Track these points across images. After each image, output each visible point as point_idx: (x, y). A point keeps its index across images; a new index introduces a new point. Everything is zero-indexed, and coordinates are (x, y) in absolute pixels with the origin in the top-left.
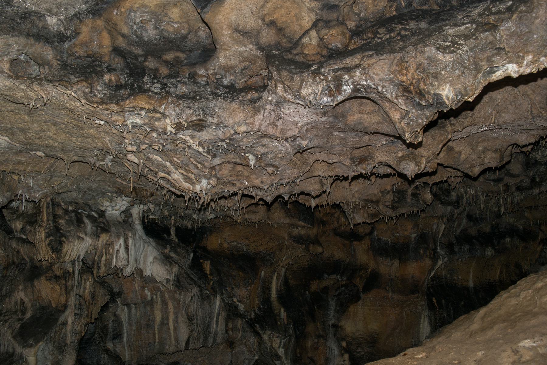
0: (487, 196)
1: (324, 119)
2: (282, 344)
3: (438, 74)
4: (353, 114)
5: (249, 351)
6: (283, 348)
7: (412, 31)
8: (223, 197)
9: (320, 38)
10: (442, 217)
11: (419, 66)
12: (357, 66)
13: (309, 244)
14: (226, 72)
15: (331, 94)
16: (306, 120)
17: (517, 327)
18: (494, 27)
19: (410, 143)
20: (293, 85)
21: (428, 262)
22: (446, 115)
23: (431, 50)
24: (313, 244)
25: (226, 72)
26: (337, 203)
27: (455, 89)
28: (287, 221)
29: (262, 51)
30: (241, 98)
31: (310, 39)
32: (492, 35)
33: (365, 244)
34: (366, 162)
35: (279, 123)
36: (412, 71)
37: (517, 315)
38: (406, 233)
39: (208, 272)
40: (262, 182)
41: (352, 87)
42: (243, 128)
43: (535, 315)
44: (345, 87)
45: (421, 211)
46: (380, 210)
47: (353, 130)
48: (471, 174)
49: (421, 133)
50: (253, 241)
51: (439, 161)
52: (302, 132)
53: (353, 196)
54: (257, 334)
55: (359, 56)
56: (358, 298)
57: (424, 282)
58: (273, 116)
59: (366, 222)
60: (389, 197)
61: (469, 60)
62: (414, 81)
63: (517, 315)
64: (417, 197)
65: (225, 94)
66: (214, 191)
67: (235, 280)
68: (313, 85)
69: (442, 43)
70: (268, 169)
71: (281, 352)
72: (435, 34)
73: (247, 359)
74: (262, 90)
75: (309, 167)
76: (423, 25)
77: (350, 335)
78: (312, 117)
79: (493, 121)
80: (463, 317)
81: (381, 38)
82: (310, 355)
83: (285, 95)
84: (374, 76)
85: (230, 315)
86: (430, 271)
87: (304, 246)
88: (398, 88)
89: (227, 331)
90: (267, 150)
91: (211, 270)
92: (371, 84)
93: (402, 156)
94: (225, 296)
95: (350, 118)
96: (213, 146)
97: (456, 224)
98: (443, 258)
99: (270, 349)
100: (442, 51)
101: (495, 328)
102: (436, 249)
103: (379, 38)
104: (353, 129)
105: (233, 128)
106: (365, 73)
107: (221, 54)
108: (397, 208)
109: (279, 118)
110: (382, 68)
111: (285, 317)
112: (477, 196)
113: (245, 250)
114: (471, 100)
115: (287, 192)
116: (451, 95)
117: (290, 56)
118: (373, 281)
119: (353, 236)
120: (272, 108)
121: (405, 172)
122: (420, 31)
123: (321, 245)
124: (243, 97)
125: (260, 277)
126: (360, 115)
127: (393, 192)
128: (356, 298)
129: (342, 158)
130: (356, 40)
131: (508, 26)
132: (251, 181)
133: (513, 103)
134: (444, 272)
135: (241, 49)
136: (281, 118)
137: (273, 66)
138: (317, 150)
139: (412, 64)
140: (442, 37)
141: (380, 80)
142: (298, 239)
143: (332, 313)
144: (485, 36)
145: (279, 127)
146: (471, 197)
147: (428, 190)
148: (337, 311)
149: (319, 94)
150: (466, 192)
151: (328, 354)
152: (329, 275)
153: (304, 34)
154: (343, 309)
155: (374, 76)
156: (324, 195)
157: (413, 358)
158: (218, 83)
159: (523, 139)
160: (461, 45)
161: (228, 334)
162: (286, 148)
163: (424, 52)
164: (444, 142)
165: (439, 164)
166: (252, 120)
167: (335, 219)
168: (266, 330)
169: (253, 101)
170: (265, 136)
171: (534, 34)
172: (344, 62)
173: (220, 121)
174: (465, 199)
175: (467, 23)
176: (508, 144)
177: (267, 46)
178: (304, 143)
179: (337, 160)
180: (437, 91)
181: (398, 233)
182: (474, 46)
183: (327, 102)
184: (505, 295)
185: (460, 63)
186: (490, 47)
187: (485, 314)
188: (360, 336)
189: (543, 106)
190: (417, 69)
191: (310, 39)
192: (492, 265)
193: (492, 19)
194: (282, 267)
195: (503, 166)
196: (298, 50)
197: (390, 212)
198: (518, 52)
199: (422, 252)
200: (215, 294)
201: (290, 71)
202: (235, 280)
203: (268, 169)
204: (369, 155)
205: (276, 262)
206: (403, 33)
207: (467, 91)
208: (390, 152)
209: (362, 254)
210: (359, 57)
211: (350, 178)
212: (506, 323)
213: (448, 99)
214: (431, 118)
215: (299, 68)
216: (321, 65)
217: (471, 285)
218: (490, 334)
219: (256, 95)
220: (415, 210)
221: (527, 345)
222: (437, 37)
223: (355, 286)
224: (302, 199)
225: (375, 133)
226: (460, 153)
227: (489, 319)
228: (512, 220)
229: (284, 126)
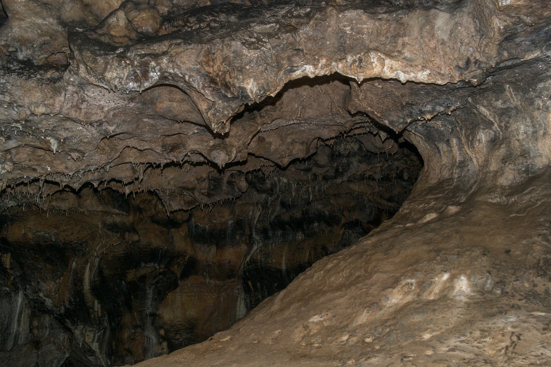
0: (298, 184)
1: (132, 105)
2: (96, 338)
3: (243, 68)
4: (163, 101)
5: (59, 349)
6: (97, 342)
7: (221, 24)
8: (22, 183)
9: (128, 19)
10: (257, 204)
11: (225, 59)
12: (164, 53)
13: (124, 232)
14: (22, 45)
15: (138, 80)
16: (113, 105)
17: (309, 306)
18: (294, 30)
19: (217, 133)
20: (96, 67)
21: (244, 247)
22: (250, 110)
23: (237, 45)
24: (129, 232)
25: (22, 45)
26: (152, 190)
27: (258, 84)
28: (100, 208)
29: (64, 27)
30: (38, 76)
31: (118, 20)
32: (293, 37)
33: (183, 231)
34: (178, 150)
35: (83, 106)
36: (218, 63)
37: (310, 294)
38: (223, 220)
39: (8, 267)
40: (67, 168)
41: (158, 74)
42: (42, 110)
43: (324, 293)
44: (152, 74)
45: (236, 198)
46: (196, 197)
47: (163, 117)
48: (280, 164)
49: (228, 124)
50: (62, 230)
51: (251, 151)
52: (108, 117)
53: (169, 184)
54: (67, 330)
55: (167, 43)
56: (176, 285)
57: (240, 267)
58: (76, 98)
59: (182, 209)
60: (205, 185)
61: (271, 57)
62: (220, 73)
63: (310, 294)
64: (233, 185)
65: (19, 69)
66: (10, 176)
67: (41, 273)
68: (118, 69)
69: (248, 38)
70: (72, 154)
71: (95, 346)
72: (242, 30)
73: (56, 358)
74: (63, 69)
75: (119, 154)
76: (233, 19)
77: (169, 322)
78: (118, 102)
79: (299, 116)
80: (267, 299)
81: (191, 27)
82: (126, 346)
83: (87, 77)
84: (181, 65)
85: (35, 312)
86: (246, 256)
87: (119, 235)
88: (205, 79)
89: (31, 330)
90: (70, 134)
91: (11, 264)
92: (178, 73)
93: (214, 145)
94: (29, 292)
95: (160, 105)
96: (6, 127)
97: (270, 211)
98: (258, 243)
99: (83, 345)
100: (247, 46)
101: (291, 308)
102: (251, 234)
103: (189, 27)
104: (163, 117)
105: (29, 108)
106: (172, 61)
107: (14, 24)
108: (213, 195)
109: (83, 101)
110: (190, 57)
111: (99, 309)
112: (289, 184)
113: (54, 240)
114: (273, 95)
115: (96, 178)
116: (255, 90)
117: (95, 36)
118: (191, 267)
119: (171, 223)
120: (74, 90)
121: (216, 162)
122: (229, 25)
123: (137, 233)
124: (41, 75)
125: (71, 268)
126: (169, 103)
127: (209, 179)
128: (173, 286)
129: (153, 145)
130: (167, 26)
131: (306, 31)
132: (54, 167)
133: (316, 100)
134: (259, 257)
135: (40, 21)
136: (85, 101)
137: (74, 45)
138: (127, 136)
139: (218, 56)
140: (249, 33)
141: (187, 69)
142: (113, 227)
143: (149, 302)
144: (286, 37)
145: (83, 111)
146: (284, 185)
147: (243, 178)
148: (154, 300)
149: (124, 79)
150: (279, 181)
151: (145, 343)
152: (146, 264)
153: (111, 14)
154: (160, 297)
155: (181, 65)
156: (136, 182)
157: (219, 342)
158: (11, 57)
159: (326, 133)
160: (265, 42)
161: (33, 334)
162: (91, 133)
163: (229, 46)
164: (254, 133)
165: (249, 154)
166: (51, 101)
167: (152, 206)
168: (77, 325)
169: (53, 81)
170: (68, 119)
171: (327, 40)
172: (152, 48)
173: (13, 100)
174: (278, 187)
175: (272, 23)
176: (313, 137)
177: (70, 22)
178: (111, 128)
179: (148, 148)
180: (242, 85)
181: (215, 219)
182: (276, 45)
183: (133, 88)
184: (302, 277)
185: (263, 59)
186: (291, 47)
187: (285, 296)
188: (179, 323)
189: (340, 105)
190: (223, 62)
191: (118, 20)
192: (302, 248)
193: (294, 21)
194: (96, 257)
195: (309, 158)
196: (105, 30)
197: (205, 200)
198: (315, 55)
199: (238, 238)
200: (16, 290)
201: (93, 53)
202: (41, 273)
203: (72, 154)
204: (181, 143)
205: (89, 252)
206: (213, 24)
207: (269, 87)
208: (202, 140)
209: (180, 241)
210: (167, 44)
211: (162, 165)
212: (300, 303)
213: (252, 93)
214: (237, 110)
215: (103, 50)
216: (127, 48)
217: (284, 267)
218: (287, 313)
219: (56, 74)
220: (231, 197)
221: (315, 320)
222: (244, 33)
223: (173, 273)
224: (113, 184)
225: (184, 121)
226: (270, 144)
227: (287, 300)
228: (320, 207)
229: (88, 109)
